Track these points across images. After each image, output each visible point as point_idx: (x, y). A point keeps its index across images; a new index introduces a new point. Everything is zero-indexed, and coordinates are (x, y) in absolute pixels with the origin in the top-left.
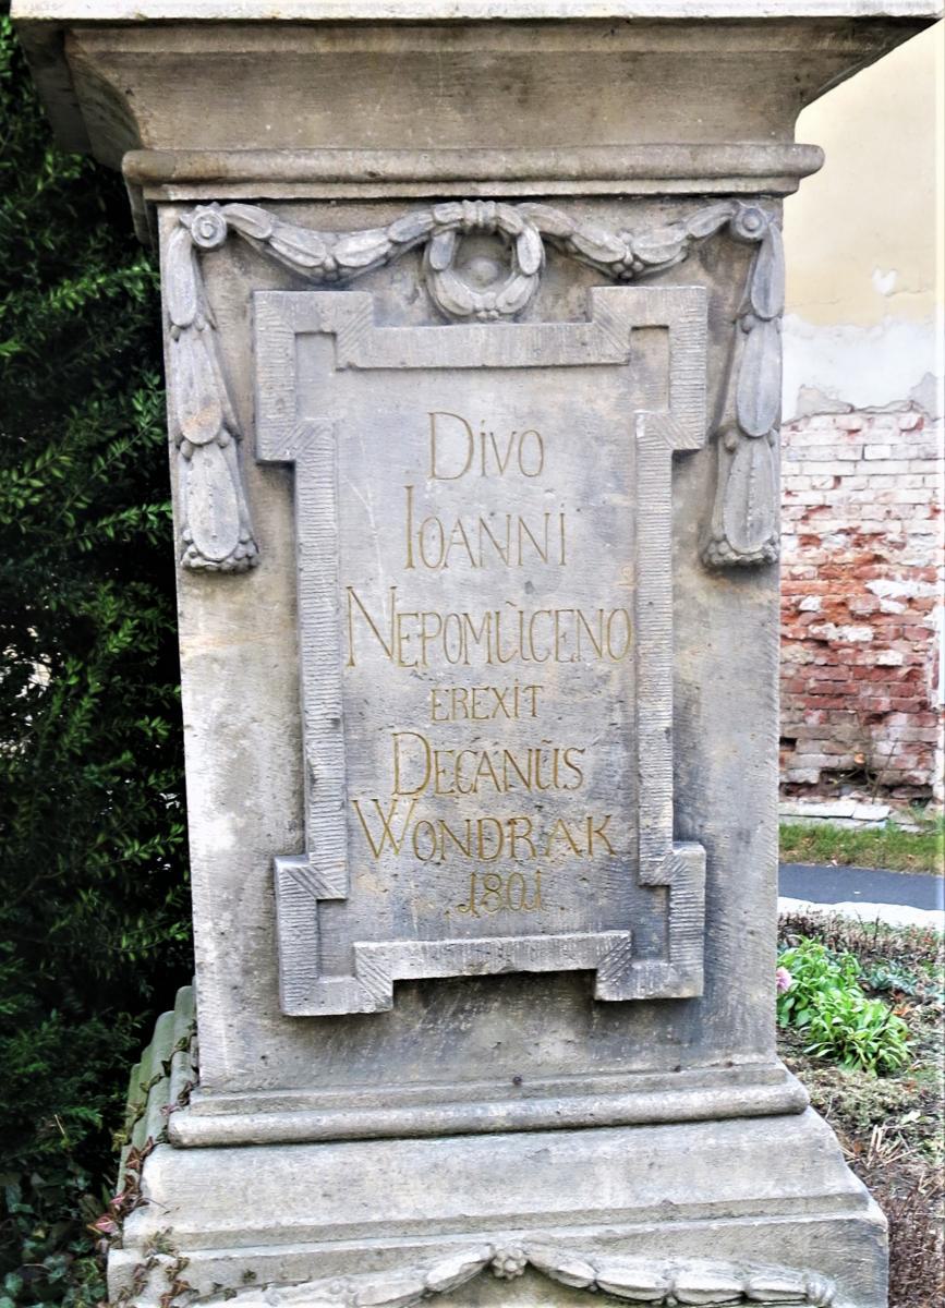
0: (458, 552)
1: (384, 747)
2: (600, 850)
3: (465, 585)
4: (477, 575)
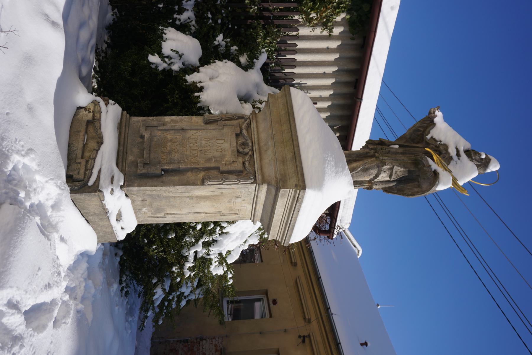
0: (206, 142)
1: (179, 134)
2: (162, 160)
3: (201, 143)
4: (203, 144)
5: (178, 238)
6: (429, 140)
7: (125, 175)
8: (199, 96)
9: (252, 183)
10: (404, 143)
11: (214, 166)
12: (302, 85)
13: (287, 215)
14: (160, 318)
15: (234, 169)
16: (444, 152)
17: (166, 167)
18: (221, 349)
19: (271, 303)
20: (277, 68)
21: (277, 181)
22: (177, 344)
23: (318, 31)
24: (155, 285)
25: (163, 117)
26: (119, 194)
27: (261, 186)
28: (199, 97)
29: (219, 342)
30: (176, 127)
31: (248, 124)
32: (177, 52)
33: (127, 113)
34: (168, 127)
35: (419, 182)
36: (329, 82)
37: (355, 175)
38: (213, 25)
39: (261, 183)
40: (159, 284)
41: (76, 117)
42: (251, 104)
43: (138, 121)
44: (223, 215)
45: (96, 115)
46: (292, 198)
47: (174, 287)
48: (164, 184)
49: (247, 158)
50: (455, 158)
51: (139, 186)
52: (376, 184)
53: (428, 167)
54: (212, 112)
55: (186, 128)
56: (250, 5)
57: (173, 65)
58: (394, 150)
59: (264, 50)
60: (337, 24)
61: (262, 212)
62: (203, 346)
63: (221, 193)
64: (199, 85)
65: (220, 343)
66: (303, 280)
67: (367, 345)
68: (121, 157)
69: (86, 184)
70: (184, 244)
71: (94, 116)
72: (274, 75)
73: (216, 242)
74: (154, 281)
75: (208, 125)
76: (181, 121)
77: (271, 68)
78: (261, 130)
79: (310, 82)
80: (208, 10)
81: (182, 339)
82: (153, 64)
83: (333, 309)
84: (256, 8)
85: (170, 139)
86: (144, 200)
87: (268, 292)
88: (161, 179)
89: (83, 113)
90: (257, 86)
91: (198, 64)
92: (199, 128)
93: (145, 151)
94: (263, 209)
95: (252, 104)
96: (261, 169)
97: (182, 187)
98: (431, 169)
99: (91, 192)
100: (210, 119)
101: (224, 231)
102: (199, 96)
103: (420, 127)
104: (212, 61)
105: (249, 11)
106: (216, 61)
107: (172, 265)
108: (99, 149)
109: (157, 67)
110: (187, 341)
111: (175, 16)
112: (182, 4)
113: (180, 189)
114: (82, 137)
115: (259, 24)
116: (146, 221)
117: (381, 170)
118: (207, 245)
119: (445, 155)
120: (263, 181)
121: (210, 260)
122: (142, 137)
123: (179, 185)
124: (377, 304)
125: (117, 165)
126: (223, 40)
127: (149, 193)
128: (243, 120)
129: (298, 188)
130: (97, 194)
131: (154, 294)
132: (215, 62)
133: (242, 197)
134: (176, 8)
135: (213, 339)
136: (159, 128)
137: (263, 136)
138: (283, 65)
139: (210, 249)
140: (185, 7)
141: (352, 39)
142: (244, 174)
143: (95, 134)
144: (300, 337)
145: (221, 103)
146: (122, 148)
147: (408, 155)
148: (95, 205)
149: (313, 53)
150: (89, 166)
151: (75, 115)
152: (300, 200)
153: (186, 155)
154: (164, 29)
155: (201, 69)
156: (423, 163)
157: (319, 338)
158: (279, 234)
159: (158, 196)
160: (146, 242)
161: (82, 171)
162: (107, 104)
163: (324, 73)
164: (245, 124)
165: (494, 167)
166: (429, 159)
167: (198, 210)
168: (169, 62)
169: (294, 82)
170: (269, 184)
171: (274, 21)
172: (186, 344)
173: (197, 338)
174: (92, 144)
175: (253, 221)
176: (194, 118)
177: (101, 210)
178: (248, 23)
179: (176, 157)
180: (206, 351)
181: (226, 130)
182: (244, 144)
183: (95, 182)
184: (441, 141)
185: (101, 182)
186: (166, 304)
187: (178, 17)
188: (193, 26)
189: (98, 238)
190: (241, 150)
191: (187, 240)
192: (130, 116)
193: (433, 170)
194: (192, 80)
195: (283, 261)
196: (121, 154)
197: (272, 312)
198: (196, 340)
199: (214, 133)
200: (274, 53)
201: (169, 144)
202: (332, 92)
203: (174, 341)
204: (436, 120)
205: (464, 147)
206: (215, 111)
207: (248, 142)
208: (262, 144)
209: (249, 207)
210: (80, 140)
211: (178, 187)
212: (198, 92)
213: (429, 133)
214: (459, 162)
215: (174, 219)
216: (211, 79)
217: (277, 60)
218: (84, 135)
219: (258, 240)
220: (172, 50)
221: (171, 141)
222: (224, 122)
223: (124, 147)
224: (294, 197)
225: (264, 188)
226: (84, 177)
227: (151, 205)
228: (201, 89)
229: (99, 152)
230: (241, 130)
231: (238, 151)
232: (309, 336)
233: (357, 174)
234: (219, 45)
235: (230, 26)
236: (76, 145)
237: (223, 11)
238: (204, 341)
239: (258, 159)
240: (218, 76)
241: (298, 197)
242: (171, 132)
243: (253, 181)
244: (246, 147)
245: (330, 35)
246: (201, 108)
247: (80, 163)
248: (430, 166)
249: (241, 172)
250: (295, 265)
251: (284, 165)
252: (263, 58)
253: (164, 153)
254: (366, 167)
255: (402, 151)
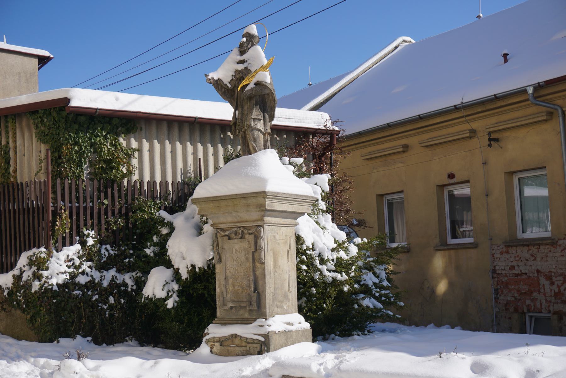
0: (235, 262)
1: (229, 281)
2: (247, 293)
3: (235, 265)
4: (236, 264)
5: (315, 284)
6: (232, 86)
7: (258, 318)
8: (199, 268)
9: (263, 228)
10: (234, 101)
11: (251, 255)
12: (182, 172)
13: (288, 201)
14: (399, 304)
15: (253, 241)
16: (241, 75)
17: (253, 290)
18: (505, 246)
19: (452, 181)
20: (168, 198)
21: (261, 211)
22: (500, 303)
23: (135, 162)
24: (360, 306)
25: (217, 294)
26: (271, 321)
27: (265, 222)
28: (200, 268)
29: (498, 249)
30: (224, 284)
31: (221, 230)
32: (164, 285)
33: (214, 320)
34: (224, 289)
35: (265, 94)
36: (179, 146)
37: (259, 148)
38: (134, 257)
39: (263, 222)
40: (360, 303)
41: (218, 354)
42: (204, 225)
43: (220, 312)
44: (290, 248)
45: (216, 340)
46: (273, 200)
47: (366, 291)
48: (264, 291)
49: (246, 232)
50: (246, 65)
51: (265, 308)
52: (266, 130)
53: (252, 91)
54: (211, 257)
55: (224, 276)
56: (117, 225)
57: (174, 289)
58: (240, 115)
59: (157, 214)
60: (128, 144)
61: (288, 218)
62: (502, 269)
63: (271, 250)
64: (190, 268)
65: (499, 248)
66: (426, 137)
67: (508, 54)
68: (246, 322)
69: (264, 342)
70: (321, 281)
71: (217, 342)
72: (175, 201)
73: (321, 254)
74: (356, 306)
75: (222, 260)
76: (219, 280)
77: (169, 204)
78: (225, 221)
79: (180, 165)
80: (123, 262)
81: (494, 296)
82: (174, 305)
83: (456, 101)
84: (120, 220)
85: (232, 288)
86: (277, 306)
87: (439, 184)
88: (261, 293)
89: (215, 350)
90: (187, 219)
91: (172, 269)
92: (224, 267)
93: (242, 305)
94: (285, 218)
95: (203, 224)
96: (254, 221)
97: (266, 278)
98: (254, 87)
99: (269, 338)
100: (217, 258)
101: (311, 247)
102: (199, 268)
103: (221, 91)
104: (167, 258)
105: (122, 226)
106: (167, 254)
107: (342, 291)
108: (240, 336)
109: (176, 302)
110: (496, 290)
111: (129, 290)
112: (119, 283)
113: (268, 279)
114: (232, 348)
115: (132, 217)
116: (295, 307)
117: (255, 128)
118: (323, 262)
119: (243, 73)
120: (262, 220)
121: (337, 259)
122: (231, 308)
123: (265, 280)
124: (477, 19)
125: (250, 324)
126: (150, 249)
127: (271, 302)
128: (218, 234)
129: (265, 196)
130: (270, 335)
131: (368, 307)
132: (169, 255)
133: (275, 234)
134: (123, 288)
135: (494, 257)
136: (225, 296)
137: (230, 219)
138: (166, 193)
139: (326, 258)
140: (122, 281)
141: (141, 129)
142: (257, 234)
143: (230, 340)
144: (490, 145)
145: (204, 251)
146: (239, 322)
147: (244, 104)
148: (279, 338)
149: (153, 164)
150: (251, 341)
151: (216, 354)
152: (275, 194)
153: (244, 276)
154: (145, 297)
155: (176, 267)
156: (250, 94)
157: (494, 120)
158: (305, 205)
159: (274, 296)
160: (321, 313)
161: (255, 345)
162: (208, 334)
163: (171, 152)
164: (221, 232)
165: (253, 29)
166: (247, 89)
167: (286, 268)
168: (172, 293)
169: (180, 181)
170: (264, 216)
171: (129, 203)
172: (499, 291)
173: (493, 278)
174: (237, 341)
175: (296, 225)
176: (217, 271)
177: (282, 335)
178: (131, 226)
179: (246, 283)
180: (507, 266)
181: (226, 247)
182: (236, 233)
183: (263, 337)
184: (233, 75)
185: (262, 333)
186: (383, 298)
187: (130, 287)
188: (136, 274)
189: (307, 341)
190: (240, 236)
191: (318, 277)
192: (216, 318)
193: (255, 86)
194: (186, 273)
195: (401, 163)
196: (244, 322)
197: (463, 180)
198: (495, 278)
199: (228, 256)
200: (156, 202)
201: (236, 288)
202: (189, 144)
203: (496, 307)
204: (216, 78)
205: (238, 56)
206: (211, 255)
207: (234, 231)
208: (236, 220)
209: (283, 229)
210: (234, 349)
211: (266, 281)
212: (196, 269)
213: (226, 85)
214: (249, 62)
215: (294, 285)
216: (184, 258)
217: (162, 199)
218: (231, 347)
219: (327, 215)
220: (163, 290)
221: (234, 287)
222: (220, 248)
223: (239, 321)
224: (272, 198)
225: (267, 219)
226: (259, 343)
227: (282, 302)
228: (193, 267)
229: (242, 336)
230: (226, 236)
231: (241, 238)
232: (489, 133)
233: (258, 146)
234: (153, 252)
235: (135, 242)
236: (238, 351)
237: (123, 249)
238: (497, 268)
239: (246, 223)
240: (181, 253)
241: (272, 196)
242: (228, 287)
243: (261, 228)
244: (238, 232)
245: (138, 150)
246: (208, 266)
247: (250, 348)
248: (252, 89)
249: (255, 236)
250: (406, 148)
251: (250, 206)
252: (164, 214)
253: (243, 292)
254: (252, 139)
255: (241, 109)
